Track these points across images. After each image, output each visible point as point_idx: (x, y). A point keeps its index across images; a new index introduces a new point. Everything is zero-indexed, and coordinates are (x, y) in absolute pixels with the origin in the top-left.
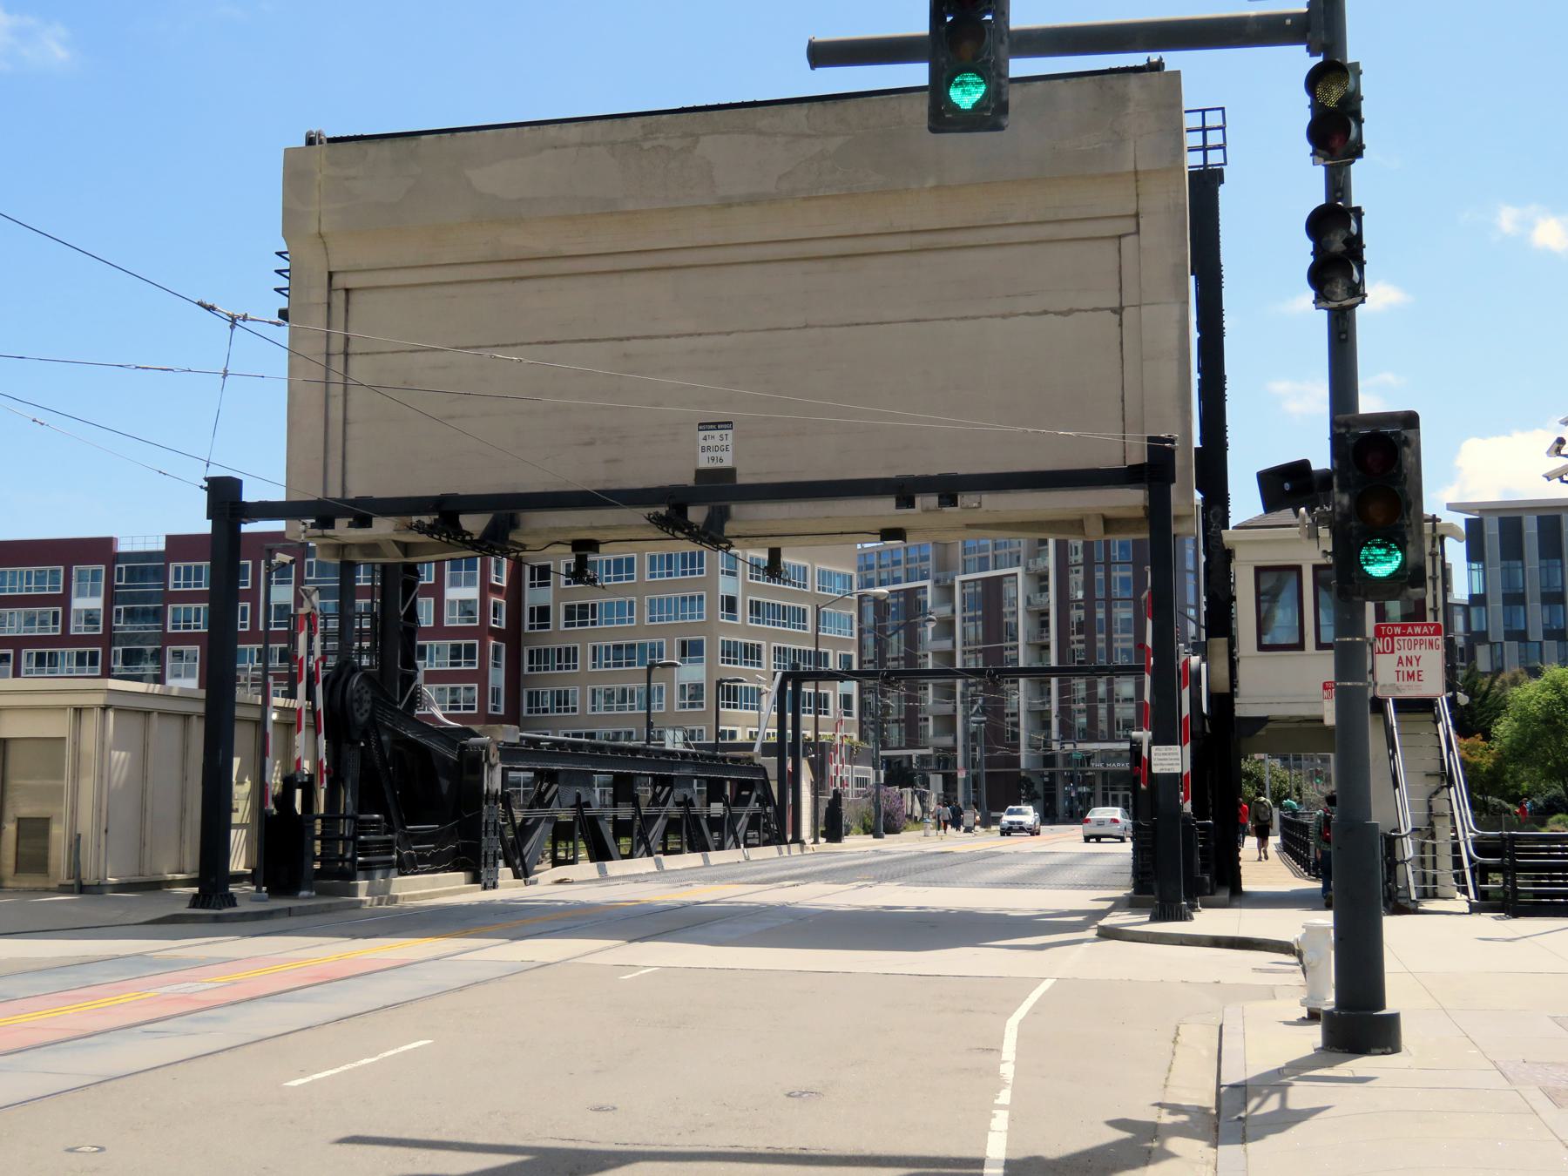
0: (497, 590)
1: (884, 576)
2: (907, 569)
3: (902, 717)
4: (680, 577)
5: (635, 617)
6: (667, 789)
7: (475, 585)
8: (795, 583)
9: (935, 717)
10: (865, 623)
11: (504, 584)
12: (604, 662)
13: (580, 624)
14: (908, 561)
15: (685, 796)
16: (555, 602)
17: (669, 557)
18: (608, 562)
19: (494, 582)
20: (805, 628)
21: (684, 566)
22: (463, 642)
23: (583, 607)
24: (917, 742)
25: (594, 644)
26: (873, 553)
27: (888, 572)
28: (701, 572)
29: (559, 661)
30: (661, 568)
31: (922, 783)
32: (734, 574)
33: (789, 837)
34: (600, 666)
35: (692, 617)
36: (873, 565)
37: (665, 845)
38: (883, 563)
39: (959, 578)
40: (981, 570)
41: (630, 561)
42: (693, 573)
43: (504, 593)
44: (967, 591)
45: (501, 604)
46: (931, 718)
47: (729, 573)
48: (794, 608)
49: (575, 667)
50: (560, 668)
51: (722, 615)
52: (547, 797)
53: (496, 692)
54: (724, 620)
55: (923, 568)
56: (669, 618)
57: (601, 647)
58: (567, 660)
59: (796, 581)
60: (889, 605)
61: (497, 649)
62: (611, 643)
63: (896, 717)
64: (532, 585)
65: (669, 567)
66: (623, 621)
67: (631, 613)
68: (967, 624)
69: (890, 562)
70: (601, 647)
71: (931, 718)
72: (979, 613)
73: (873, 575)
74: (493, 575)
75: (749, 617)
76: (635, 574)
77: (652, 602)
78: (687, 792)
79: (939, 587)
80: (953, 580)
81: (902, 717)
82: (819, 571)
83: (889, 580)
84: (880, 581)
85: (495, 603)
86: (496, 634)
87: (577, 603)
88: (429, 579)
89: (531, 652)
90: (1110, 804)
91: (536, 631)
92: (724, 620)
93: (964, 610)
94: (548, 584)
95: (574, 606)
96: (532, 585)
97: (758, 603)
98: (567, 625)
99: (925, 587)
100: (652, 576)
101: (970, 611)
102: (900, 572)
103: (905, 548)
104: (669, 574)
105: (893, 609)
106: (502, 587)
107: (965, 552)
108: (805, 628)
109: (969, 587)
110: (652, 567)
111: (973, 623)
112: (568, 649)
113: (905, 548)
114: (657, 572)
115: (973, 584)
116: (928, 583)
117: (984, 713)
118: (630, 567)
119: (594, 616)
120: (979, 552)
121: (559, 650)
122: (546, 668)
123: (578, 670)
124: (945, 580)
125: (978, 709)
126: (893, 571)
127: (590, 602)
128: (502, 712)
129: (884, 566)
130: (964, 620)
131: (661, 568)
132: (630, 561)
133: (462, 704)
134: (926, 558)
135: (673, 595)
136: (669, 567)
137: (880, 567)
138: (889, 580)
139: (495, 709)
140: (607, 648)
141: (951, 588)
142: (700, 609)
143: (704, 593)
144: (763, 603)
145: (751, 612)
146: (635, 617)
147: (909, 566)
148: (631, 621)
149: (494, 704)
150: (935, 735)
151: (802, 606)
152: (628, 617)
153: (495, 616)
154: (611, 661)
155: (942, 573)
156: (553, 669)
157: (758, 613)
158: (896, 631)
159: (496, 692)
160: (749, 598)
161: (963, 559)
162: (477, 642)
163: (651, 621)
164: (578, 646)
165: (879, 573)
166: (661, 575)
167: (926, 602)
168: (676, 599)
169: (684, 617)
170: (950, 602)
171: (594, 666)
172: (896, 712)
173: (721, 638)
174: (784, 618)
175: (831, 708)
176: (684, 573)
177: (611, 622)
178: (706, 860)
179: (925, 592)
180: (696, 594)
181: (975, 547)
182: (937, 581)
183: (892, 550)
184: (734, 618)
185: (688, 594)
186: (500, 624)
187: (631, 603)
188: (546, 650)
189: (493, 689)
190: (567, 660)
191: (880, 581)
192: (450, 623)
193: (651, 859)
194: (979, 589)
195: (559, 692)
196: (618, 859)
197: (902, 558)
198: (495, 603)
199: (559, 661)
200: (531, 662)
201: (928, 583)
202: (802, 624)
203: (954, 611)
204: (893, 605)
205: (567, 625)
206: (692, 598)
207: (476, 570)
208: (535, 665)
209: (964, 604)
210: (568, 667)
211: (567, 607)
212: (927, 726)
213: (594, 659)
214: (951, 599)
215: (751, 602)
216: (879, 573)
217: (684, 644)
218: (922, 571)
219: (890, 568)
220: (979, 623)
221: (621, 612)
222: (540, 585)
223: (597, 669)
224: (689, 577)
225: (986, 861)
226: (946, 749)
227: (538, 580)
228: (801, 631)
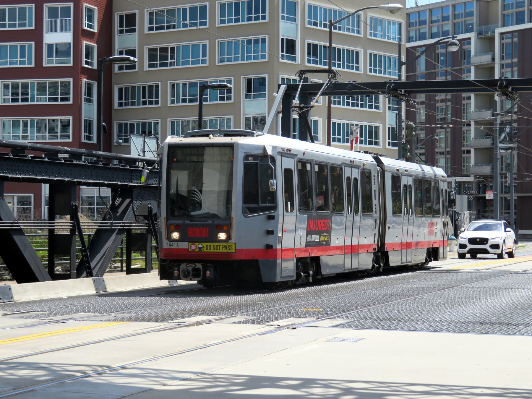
0: (89, 35)
1: (435, 30)
2: (455, 24)
3: (449, 149)
4: (246, 23)
5: (207, 58)
6: (128, 201)
7: (69, 30)
8: (349, 29)
9: (476, 150)
10: (418, 70)
11: (96, 30)
12: (181, 97)
13: (161, 65)
14: (455, 16)
15: (150, 210)
16: (139, 46)
17: (237, 4)
18: (185, 10)
19: (86, 28)
20: (358, 69)
21: (249, 12)
22: (59, 80)
23: (164, 50)
24: (460, 170)
25: (173, 82)
26: (425, 10)
27: (438, 26)
28: (264, 18)
29: (144, 97)
30: (230, 15)
31: (151, 172)
32: (295, 20)
33: (69, 272)
34: (178, 102)
35: (256, 57)
36: (426, 20)
37: (51, 266)
38: (434, 18)
39: (498, 31)
40: (517, 23)
41: (203, 9)
42: (257, 18)
43: (96, 37)
44: (505, 41)
45: (92, 48)
46: (472, 151)
47: (288, 19)
48: (348, 51)
49: (157, 102)
50: (144, 103)
51: (283, 56)
52: (120, 210)
53: (89, 124)
54: (285, 61)
55: (468, 22)
56: (236, 59)
57: (178, 85)
58: (151, 97)
59: (350, 27)
60: (438, 54)
61: (89, 88)
62: (187, 81)
63: (444, 150)
64: (121, 32)
65: (237, 13)
66: (198, 62)
67: (204, 55)
68: (505, 70)
69: (440, 18)
70: (178, 85)
71: (472, 151)
72: (515, 60)
73: (425, 29)
74: (85, 22)
75: (306, 57)
76: (207, 20)
77: (221, 44)
78: (153, 204)
79: (481, 38)
80: (493, 32)
81: (449, 149)
82: (371, 18)
83: (439, 32)
84: (432, 34)
85: (87, 47)
86: (89, 73)
87: (158, 46)
88: (30, 25)
89: (121, 90)
90: (162, 263)
91: (124, 71)
92: (285, 61)
93: (502, 58)
94: (134, 31)
95: (155, 49)
96: (121, 32)
97: (315, 46)
98: (150, 66)
99: (470, 39)
100: (222, 22)
101: (508, 59)
102: (448, 27)
103: (453, 5)
104: (237, 20)
105: (442, 58)
106: (94, 33)
107: (504, 7)
108: (358, 69)
109: (506, 39)
110: (222, 15)
111: (510, 69)
112: (151, 87)
113: (453, 5)
114: (226, 18)
115: (510, 35)
116: (472, 35)
117: (511, 141)
118: (203, 15)
119: (172, 58)
120: (517, 7)
121: (144, 88)
122: (133, 104)
123: (159, 105)
124: (487, 33)
125: (505, 137)
126: (442, 25)
127: (170, 45)
128: (95, 141)
129: (435, 21)
130: (502, 66)
131: (230, 15)
132: (203, 9)
133: (59, 134)
134: (471, 14)
135: (240, 38)
136: (237, 13)
137: (432, 22)
138: (439, 32)
139: (89, 138)
140: (184, 85)
141: (492, 39)
142: (263, 49)
143: (267, 37)
144: (320, 46)
145: (309, 54)
146: (207, 58)
147: (456, 21)
148: (204, 61)
149: (87, 134)
150: (476, 164)
151: (356, 49)
152: (201, 58)
153: (87, 57)
154: (187, 97)
155: (484, 27)
156: (138, 104)
157: (315, 55)
158: (508, 128)
159: (89, 124)
160: (307, 41)
161: (502, 14)
162: (71, 80)
163: (221, 62)
164: (160, 84)
165: (431, 28)
166: (230, 21)
167: (470, 52)
168: (243, 41)
169: (249, 58)
170: (490, 51)
171: (173, 101)
172: (443, 145)
173: (281, 76)
174: (339, 60)
175: (381, 140)
176: (249, 19)
177: (188, 63)
178: (100, 286)
179: (469, 43)
180: (260, 37)
181: (512, 4)
182: (479, 34)
183: (442, 8)
184: (294, 59)
185: (253, 38)
186: (92, 64)
187: (204, 46)
188: (133, 88)
189: (86, 121)
190: (151, 97)
191: (432, 34)
192: (48, 63)
193: (90, 279)
194: (516, 40)
195: (144, 124)
196: (45, 280)
197: (450, 14)
198: (87, 47)
199: (144, 97)
200: (120, 98)
201: (472, 35)
202: (355, 65)
203: (493, 59)
204: (442, 55)
205: (150, 66)
206: (256, 41)
207: (70, 17)
208: (124, 101)
209: (503, 53)
210: (151, 103)
211: (150, 50)
212: (469, 157)
213: (173, 96)
214: (492, 49)
215: (309, 45)
216: (431, 28)
217: (249, 81)
218: (467, 25)
219: (440, 23)
220: (515, 69)
221: (195, 55)
222: (128, 31)
223: (176, 105)
224: (253, 22)
225: (485, 284)
226: (486, 177)
227: (126, 27)
228: (354, 71)
